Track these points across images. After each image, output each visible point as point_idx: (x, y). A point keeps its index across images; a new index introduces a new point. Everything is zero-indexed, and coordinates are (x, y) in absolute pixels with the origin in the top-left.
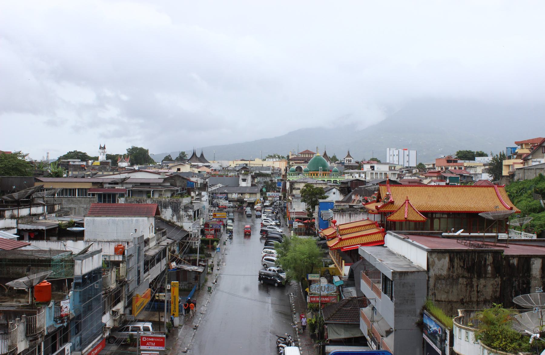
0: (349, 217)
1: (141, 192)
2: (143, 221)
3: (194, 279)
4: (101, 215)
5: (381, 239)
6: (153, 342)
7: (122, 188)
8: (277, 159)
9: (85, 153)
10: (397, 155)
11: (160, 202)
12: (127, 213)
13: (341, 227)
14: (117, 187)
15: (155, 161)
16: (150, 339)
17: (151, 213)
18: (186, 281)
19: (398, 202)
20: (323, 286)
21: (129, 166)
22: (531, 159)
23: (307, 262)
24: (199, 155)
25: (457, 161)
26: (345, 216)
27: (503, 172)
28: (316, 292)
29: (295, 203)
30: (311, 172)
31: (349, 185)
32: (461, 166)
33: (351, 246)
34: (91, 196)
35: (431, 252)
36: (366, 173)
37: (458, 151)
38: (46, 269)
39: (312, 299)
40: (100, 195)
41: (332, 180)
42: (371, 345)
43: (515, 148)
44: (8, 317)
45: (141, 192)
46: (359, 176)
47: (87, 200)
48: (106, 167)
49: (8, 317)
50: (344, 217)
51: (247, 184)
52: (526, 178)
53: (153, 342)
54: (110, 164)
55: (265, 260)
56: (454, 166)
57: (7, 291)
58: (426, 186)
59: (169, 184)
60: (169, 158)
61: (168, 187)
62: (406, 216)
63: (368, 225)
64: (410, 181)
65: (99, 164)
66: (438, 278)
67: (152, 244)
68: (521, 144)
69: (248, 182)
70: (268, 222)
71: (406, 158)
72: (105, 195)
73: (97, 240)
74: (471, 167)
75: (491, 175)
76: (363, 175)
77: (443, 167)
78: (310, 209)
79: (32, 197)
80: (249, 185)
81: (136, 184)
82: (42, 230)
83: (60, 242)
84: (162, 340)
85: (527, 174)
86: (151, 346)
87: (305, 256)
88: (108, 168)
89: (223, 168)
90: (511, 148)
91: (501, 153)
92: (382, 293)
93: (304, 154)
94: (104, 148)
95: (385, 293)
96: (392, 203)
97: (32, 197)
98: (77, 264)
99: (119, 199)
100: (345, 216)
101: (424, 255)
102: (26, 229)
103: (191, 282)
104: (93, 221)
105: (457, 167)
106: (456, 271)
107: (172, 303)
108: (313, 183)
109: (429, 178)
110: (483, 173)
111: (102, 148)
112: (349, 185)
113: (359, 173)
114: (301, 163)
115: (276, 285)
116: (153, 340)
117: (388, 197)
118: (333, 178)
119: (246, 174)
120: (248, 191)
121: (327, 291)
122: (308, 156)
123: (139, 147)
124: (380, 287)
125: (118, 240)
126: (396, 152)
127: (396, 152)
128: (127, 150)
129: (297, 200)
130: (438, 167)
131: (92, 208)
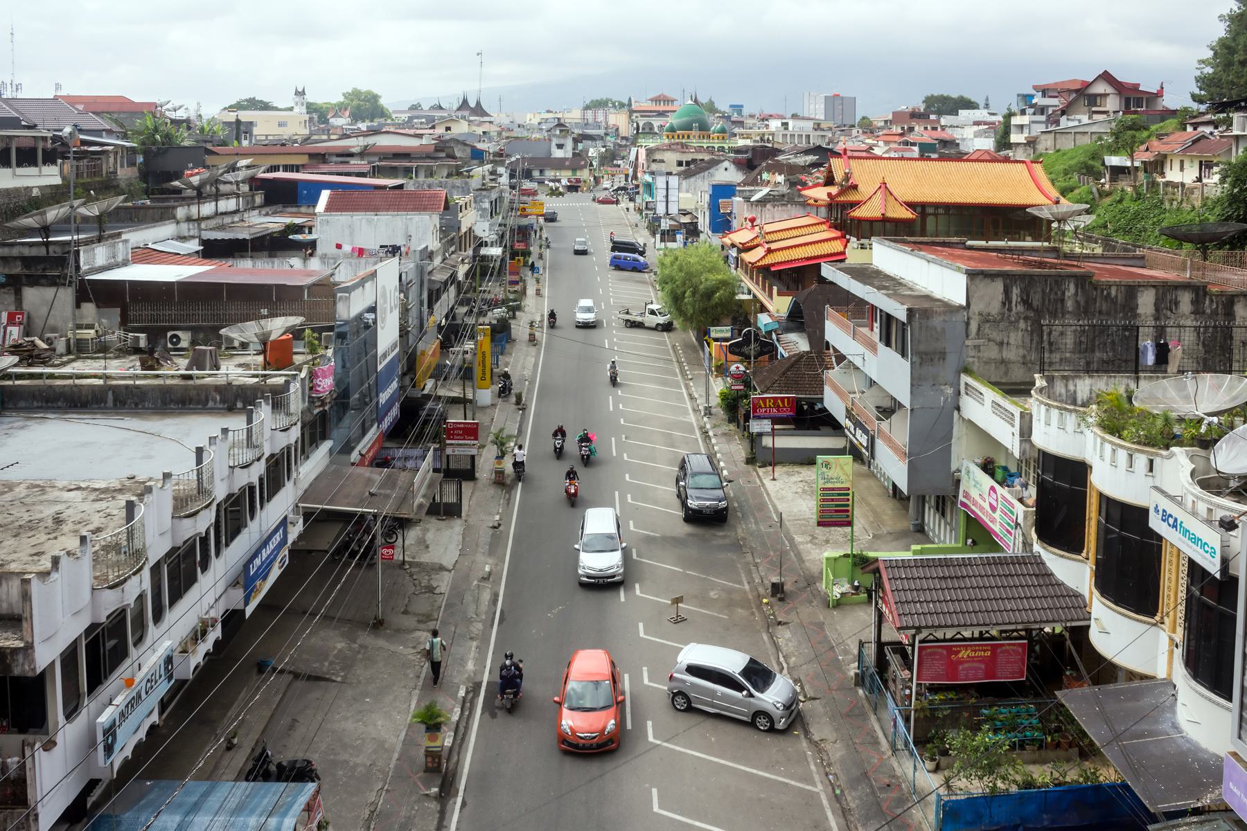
5: (841, 249)
13: (768, 228)
19: (865, 189)
24: (472, 104)
35: (972, 275)
42: (854, 436)
43: (1032, 96)
51: (565, 152)
58: (881, 158)
66: (986, 319)
67: (437, 261)
68: (1045, 92)
80: (570, 155)
85: (1058, 141)
92: (881, 347)
94: (303, 93)
95: (888, 344)
101: (962, 280)
106: (1014, 308)
110: (975, 137)
114: (653, 116)
117: (847, 177)
124: (876, 335)
128: (344, 95)
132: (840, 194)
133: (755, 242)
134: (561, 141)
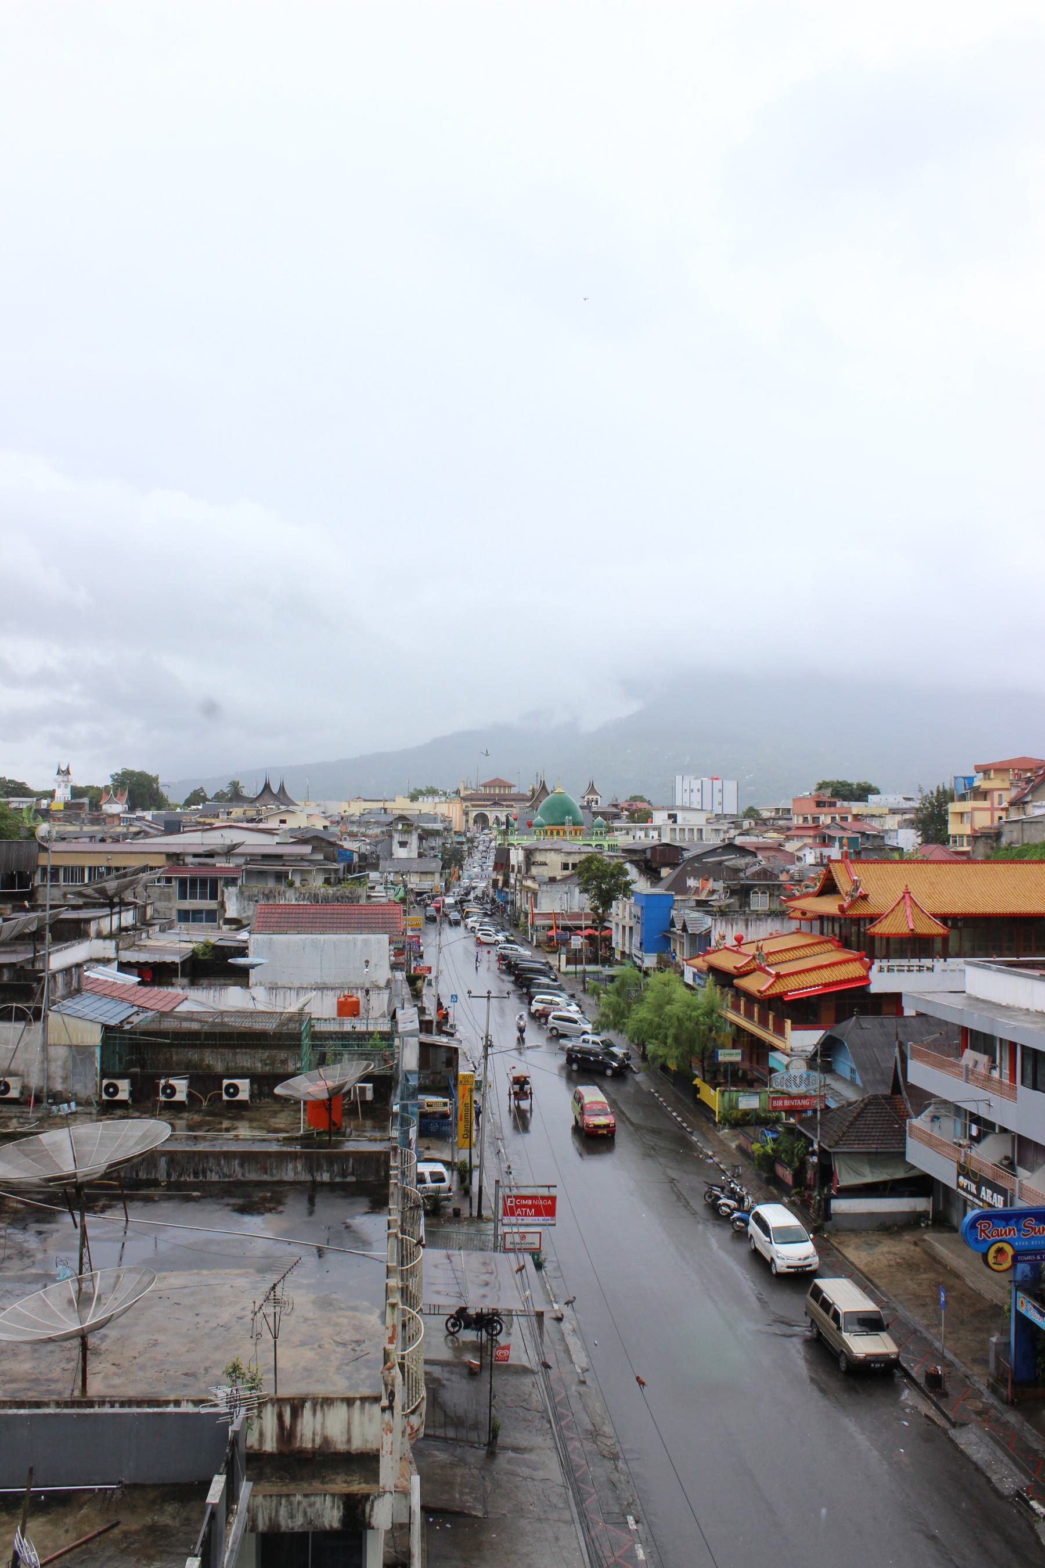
0: (744, 927)
1: (262, 874)
2: (379, 942)
3: (444, 1065)
4: (285, 929)
5: (863, 972)
6: (530, 1207)
7: (227, 865)
8: (443, 799)
9: (24, 783)
10: (698, 790)
11: (315, 895)
12: (342, 925)
14: (220, 863)
15: (170, 801)
16: (524, 1202)
17: (394, 925)
18: (428, 1068)
20: (798, 1075)
21: (124, 812)
22: (1031, 801)
23: (704, 1024)
24: (275, 789)
25: (835, 803)
26: (737, 924)
27: (950, 826)
28: (785, 1087)
29: (545, 894)
30: (546, 828)
31: (649, 855)
32: (846, 813)
33: (803, 989)
34: (163, 884)
36: (660, 829)
37: (821, 782)
38: (253, 1052)
39: (774, 1102)
40: (182, 882)
41: (594, 844)
44: (315, 1166)
45: (262, 874)
46: (646, 836)
47: (155, 892)
48: (79, 814)
49: (315, 1166)
50: (734, 926)
51: (410, 852)
52: (1026, 842)
53: (530, 1207)
54: (87, 808)
55: (554, 1018)
56: (831, 813)
57: (205, 1104)
59: (320, 857)
60: (199, 795)
61: (321, 863)
62: (912, 927)
63: (809, 945)
64: (760, 846)
65: (62, 808)
69: (412, 848)
70: (490, 935)
71: (718, 797)
72: (193, 881)
73: (277, 984)
74: (873, 816)
75: (919, 833)
76: (655, 834)
77: (809, 816)
78: (597, 908)
79: (33, 885)
80: (415, 855)
81: (252, 858)
82: (173, 963)
83: (212, 991)
84: (550, 1202)
85: (1027, 833)
86: (526, 1215)
87: (699, 1011)
88: (83, 816)
89: (342, 818)
90: (964, 778)
91: (938, 787)
93: (490, 787)
94: (67, 772)
96: (864, 897)
97: (33, 885)
98: (409, 1046)
99: (225, 890)
100: (737, 924)
102: (138, 963)
103: (438, 1071)
104: (270, 943)
105: (837, 816)
107: (461, 1120)
108: (574, 851)
109: (795, 839)
110: (900, 828)
111: (63, 772)
112: (649, 855)
113: (646, 829)
114: (486, 806)
115: (609, 1072)
116: (530, 1202)
117: (856, 885)
118: (596, 840)
119: (407, 832)
120: (415, 867)
121: (807, 1085)
122: (500, 791)
123: (137, 770)
125: (324, 983)
126: (696, 785)
127: (696, 785)
129: (549, 889)
130: (798, 815)
131: (262, 915)
132: (852, 904)
133: (753, 966)
134: (404, 838)
